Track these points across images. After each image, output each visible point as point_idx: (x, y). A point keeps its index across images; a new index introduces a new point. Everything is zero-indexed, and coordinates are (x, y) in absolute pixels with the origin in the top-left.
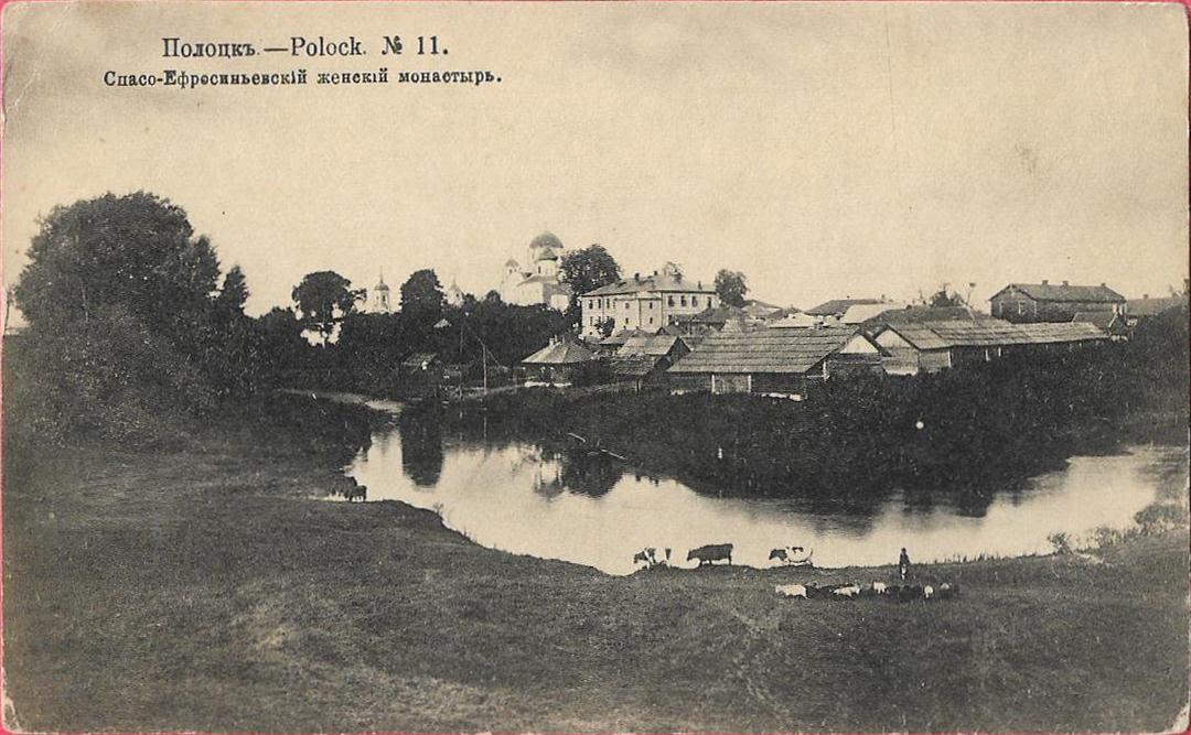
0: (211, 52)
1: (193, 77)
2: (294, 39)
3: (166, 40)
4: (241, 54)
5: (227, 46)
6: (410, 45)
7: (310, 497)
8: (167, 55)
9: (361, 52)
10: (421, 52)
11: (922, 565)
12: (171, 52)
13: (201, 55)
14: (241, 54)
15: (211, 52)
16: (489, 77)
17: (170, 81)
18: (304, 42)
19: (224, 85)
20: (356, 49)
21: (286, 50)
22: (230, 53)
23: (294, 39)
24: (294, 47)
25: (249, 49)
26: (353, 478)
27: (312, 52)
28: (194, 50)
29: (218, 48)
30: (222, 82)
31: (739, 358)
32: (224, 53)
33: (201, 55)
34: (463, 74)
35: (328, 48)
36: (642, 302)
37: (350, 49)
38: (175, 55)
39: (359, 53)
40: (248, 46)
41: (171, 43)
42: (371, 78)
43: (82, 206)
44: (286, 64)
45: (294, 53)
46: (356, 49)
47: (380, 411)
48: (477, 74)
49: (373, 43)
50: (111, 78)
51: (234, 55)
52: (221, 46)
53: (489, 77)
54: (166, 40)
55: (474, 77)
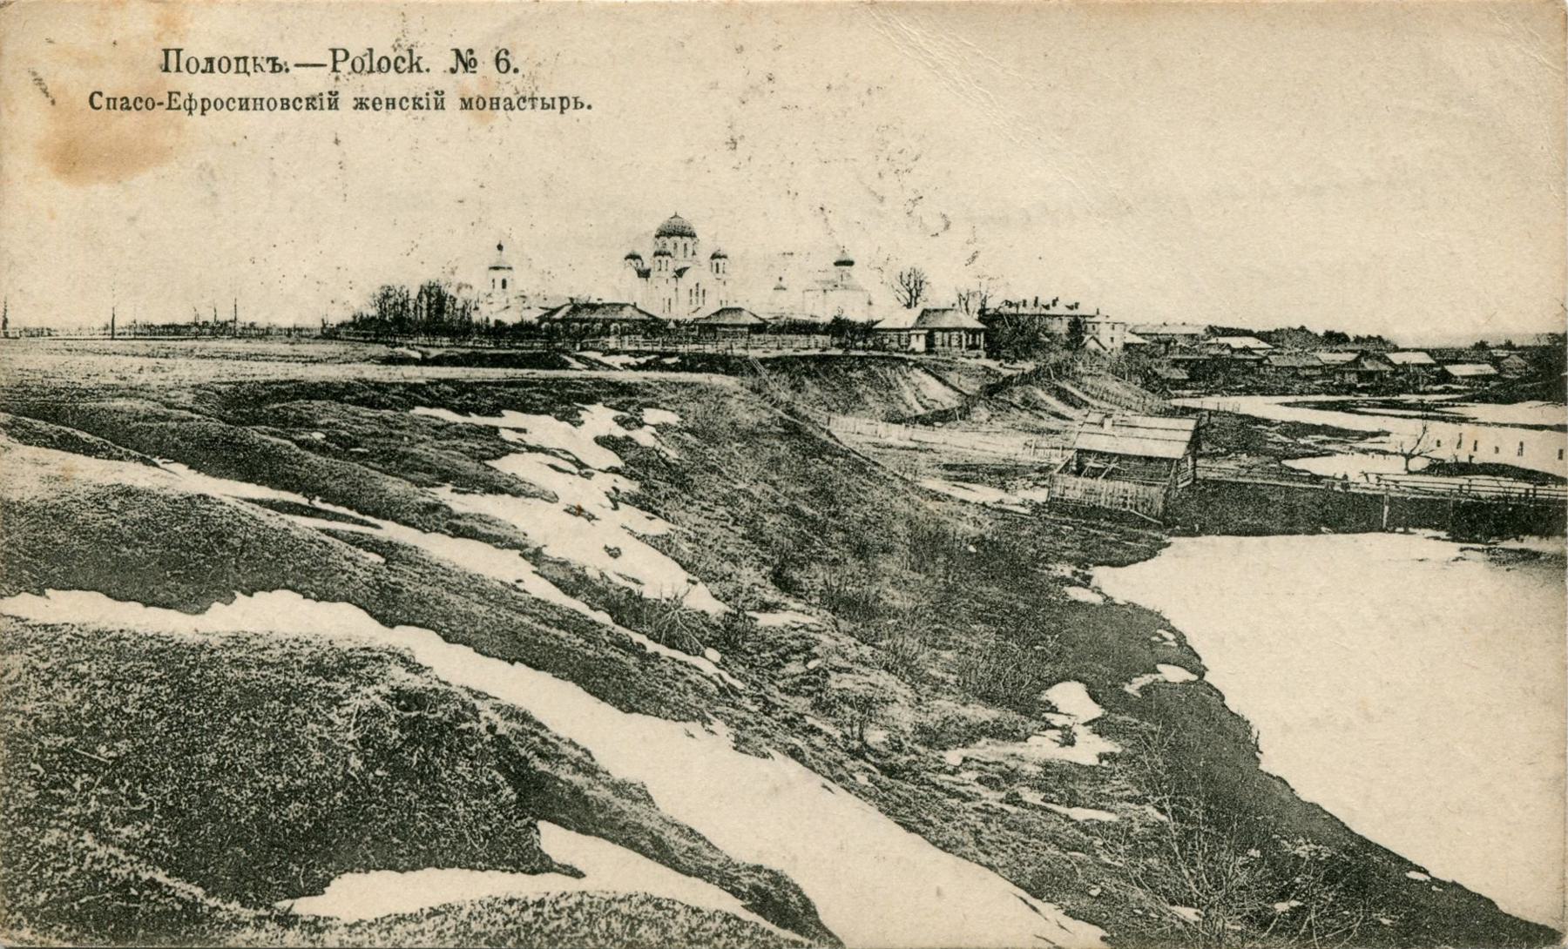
0: (224, 68)
2: (334, 51)
5: (245, 59)
6: (485, 59)
7: (672, 418)
8: (166, 70)
9: (423, 67)
12: (172, 66)
15: (224, 68)
16: (578, 104)
17: (174, 105)
18: (396, 69)
19: (243, 113)
20: (415, 66)
21: (1520, 453)
22: (250, 68)
23: (334, 51)
24: (335, 62)
26: (980, 320)
28: (203, 65)
31: (627, 366)
32: (241, 68)
33: (212, 71)
37: (407, 64)
38: (178, 70)
39: (419, 70)
40: (274, 59)
41: (173, 55)
42: (424, 103)
44: (318, 82)
45: (334, 70)
46: (415, 66)
47: (715, 371)
48: (562, 99)
49: (438, 59)
50: (98, 100)
52: (238, 59)
53: (578, 104)
55: (557, 102)
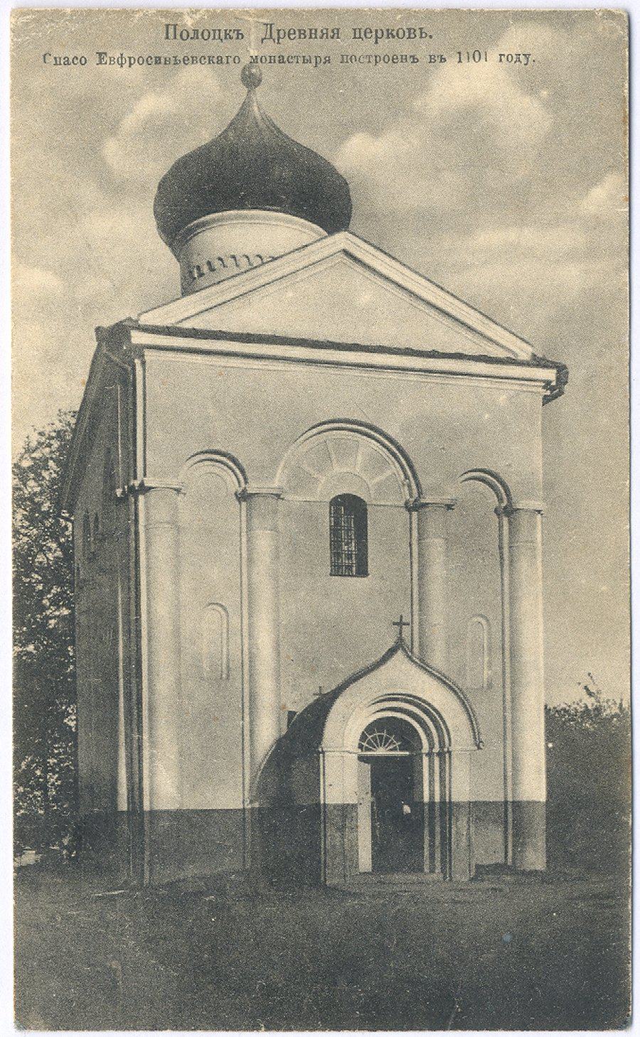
1: (130, 58)
3: (355, 30)
4: (231, 38)
8: (167, 38)
10: (167, 38)
11: (380, 719)
13: (197, 38)
14: (231, 38)
25: (238, 34)
27: (510, 56)
29: (212, 32)
30: (156, 63)
34: (304, 57)
35: (203, 33)
36: (260, 262)
40: (238, 30)
43: (21, 1022)
51: (226, 38)
54: (355, 30)
55: (313, 60)
